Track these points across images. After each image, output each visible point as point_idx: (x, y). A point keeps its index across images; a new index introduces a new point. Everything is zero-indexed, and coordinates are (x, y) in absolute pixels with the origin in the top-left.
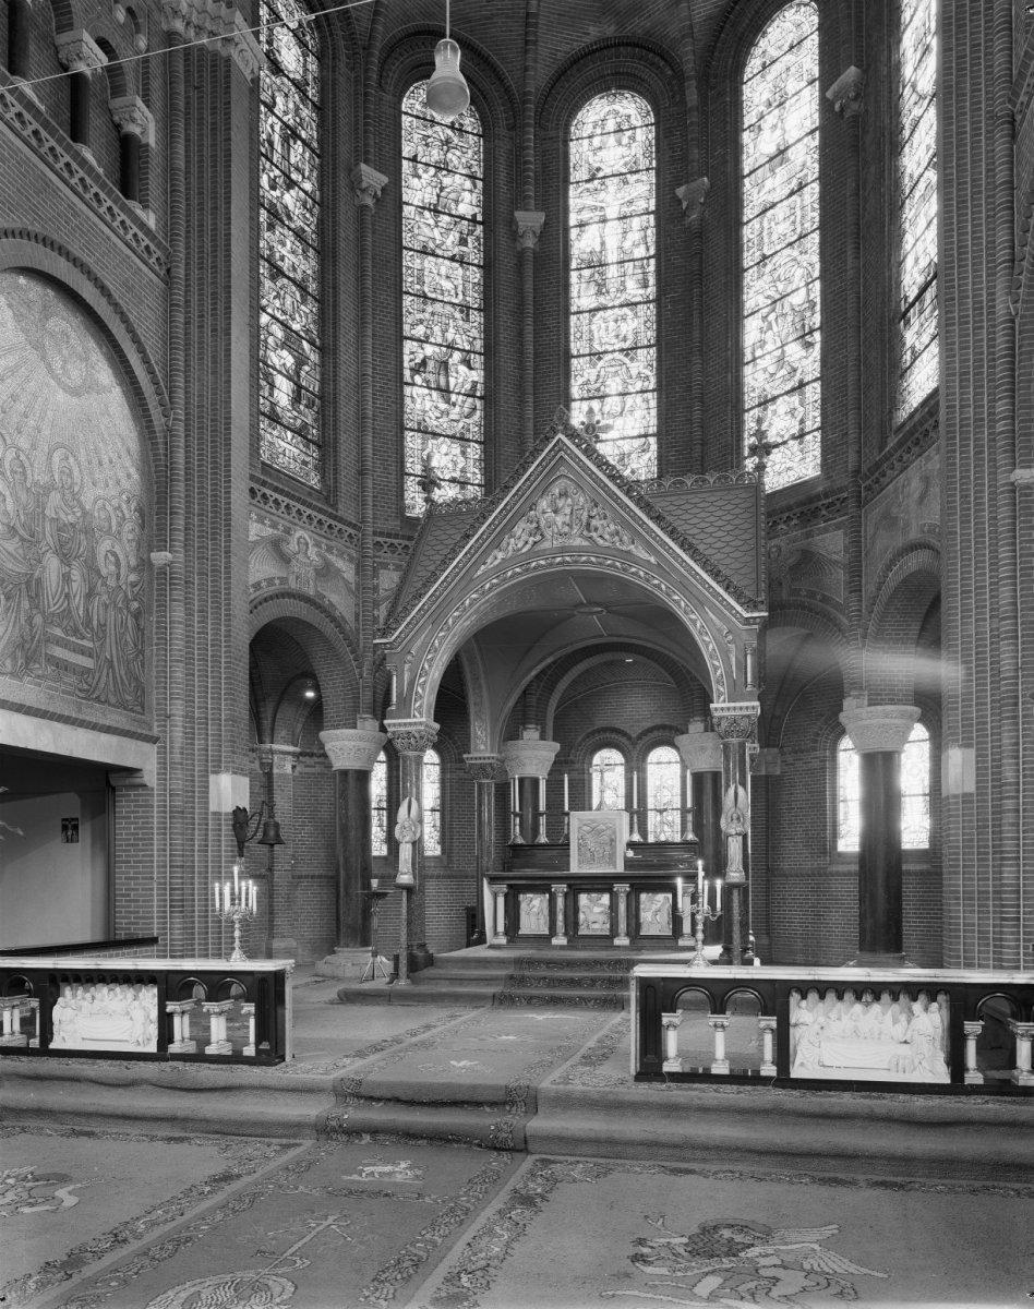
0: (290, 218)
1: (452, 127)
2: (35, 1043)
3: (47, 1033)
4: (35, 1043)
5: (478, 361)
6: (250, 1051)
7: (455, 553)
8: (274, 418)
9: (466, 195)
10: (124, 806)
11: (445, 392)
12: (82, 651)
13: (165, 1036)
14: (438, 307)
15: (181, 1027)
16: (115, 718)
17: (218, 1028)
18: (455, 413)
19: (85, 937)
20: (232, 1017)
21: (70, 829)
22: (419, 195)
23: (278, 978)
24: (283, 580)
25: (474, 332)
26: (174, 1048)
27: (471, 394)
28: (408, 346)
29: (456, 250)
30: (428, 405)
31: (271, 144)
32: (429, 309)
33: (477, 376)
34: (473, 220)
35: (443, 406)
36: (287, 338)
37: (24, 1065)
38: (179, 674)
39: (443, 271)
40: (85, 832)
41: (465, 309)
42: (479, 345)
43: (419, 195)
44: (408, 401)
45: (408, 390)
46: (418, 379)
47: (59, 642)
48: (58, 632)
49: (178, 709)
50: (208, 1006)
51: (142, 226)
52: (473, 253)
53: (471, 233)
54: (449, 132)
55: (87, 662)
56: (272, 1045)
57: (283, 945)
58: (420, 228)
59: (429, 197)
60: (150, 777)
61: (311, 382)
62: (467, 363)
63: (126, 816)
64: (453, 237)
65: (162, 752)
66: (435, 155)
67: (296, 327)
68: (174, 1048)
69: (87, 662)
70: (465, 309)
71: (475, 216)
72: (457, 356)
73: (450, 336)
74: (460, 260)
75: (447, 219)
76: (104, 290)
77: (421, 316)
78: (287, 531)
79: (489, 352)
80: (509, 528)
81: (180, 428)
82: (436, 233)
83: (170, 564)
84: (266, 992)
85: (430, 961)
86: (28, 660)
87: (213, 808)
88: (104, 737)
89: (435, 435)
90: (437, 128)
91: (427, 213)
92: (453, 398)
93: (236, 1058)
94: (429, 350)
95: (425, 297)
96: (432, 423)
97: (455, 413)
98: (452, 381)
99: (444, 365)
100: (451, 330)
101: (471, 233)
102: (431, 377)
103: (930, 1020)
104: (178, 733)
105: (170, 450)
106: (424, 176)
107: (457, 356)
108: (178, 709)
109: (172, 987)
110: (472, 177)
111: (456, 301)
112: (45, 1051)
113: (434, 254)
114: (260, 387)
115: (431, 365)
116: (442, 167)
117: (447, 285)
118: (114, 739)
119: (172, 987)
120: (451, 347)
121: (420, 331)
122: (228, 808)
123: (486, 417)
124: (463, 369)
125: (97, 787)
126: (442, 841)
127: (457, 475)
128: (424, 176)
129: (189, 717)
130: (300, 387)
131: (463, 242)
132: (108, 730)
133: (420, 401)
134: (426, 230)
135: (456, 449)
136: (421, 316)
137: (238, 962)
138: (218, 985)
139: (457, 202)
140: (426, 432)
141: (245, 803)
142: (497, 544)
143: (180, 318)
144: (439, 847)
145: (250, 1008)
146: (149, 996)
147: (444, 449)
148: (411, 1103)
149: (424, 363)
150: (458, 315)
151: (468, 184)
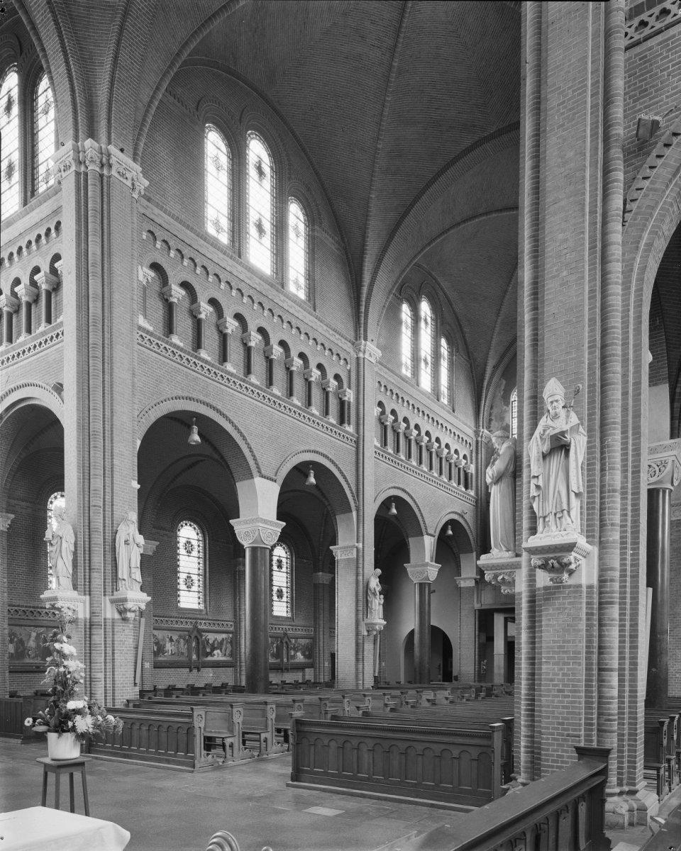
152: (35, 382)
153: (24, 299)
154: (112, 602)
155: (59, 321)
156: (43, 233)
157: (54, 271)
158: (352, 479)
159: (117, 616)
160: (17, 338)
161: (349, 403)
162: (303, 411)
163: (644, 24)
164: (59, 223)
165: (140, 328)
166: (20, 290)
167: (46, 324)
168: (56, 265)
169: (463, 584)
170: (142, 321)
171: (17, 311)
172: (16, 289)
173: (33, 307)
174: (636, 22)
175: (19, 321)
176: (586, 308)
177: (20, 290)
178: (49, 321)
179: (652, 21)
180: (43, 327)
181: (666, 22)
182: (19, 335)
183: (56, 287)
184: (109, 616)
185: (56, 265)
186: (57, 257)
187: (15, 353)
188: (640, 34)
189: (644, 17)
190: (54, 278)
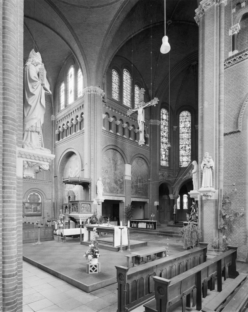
0: (164, 136)
1: (187, 116)
2: (137, 227)
3: (138, 226)
4: (137, 227)
5: (190, 145)
6: (153, 228)
7: (182, 174)
8: (162, 160)
9: (189, 124)
10: (146, 205)
11: (185, 150)
12: (141, 191)
13: (147, 227)
14: (185, 140)
15: (148, 226)
16: (144, 197)
17: (151, 226)
18: (187, 153)
19: (142, 219)
20: (152, 226)
21: (141, 207)
22: (182, 126)
23: (156, 222)
24: (163, 179)
25: (190, 142)
26: (147, 228)
27: (189, 150)
28: (180, 146)
29: (187, 132)
30: (183, 152)
31: (162, 129)
32: (183, 140)
33: (190, 147)
34: (190, 127)
35: (185, 152)
36: (164, 150)
37: (136, 229)
38: (151, 191)
39: (185, 135)
40: (142, 208)
41: (188, 139)
42: (190, 143)
43: (182, 126)
44: (180, 152)
45: (180, 151)
46: (182, 149)
47: (139, 190)
48: (139, 190)
49: (151, 195)
50: (150, 225)
51: (147, 147)
52: (190, 131)
53: (189, 129)
54: (186, 117)
55: (142, 192)
56: (155, 228)
57: (166, 220)
58: (182, 130)
59: (183, 126)
60: (148, 202)
61: (167, 154)
62: (189, 146)
63: (146, 207)
64: (187, 130)
65: (149, 200)
66: (184, 120)
67: (165, 148)
68: (147, 228)
69: (142, 192)
70: (188, 139)
71: (190, 126)
72: (187, 145)
73: (186, 143)
74: (188, 133)
75: (186, 128)
76: (144, 155)
77: (182, 141)
78: (164, 173)
79: (192, 144)
80: (186, 174)
81: (151, 166)
82: (184, 130)
83: (150, 180)
84: (155, 223)
85: (178, 222)
86: (137, 193)
87: (155, 205)
88: (144, 199)
89: (184, 156)
90: (185, 117)
91: (183, 128)
92: (187, 151)
93: (152, 229)
94: (183, 145)
95: (183, 139)
96: (184, 155)
97: (187, 153)
98: (186, 149)
99: (185, 147)
100: (186, 142)
101: (189, 129)
102: (184, 149)
103: (145, 224)
104: (151, 197)
105: (150, 168)
106: (183, 124)
107: (187, 145)
108: (151, 195)
109: (148, 223)
110: (189, 122)
111: (187, 138)
112: (138, 228)
113: (184, 133)
114: (160, 157)
115: (183, 147)
116: (186, 121)
117: (186, 136)
118: (144, 199)
119: (148, 223)
120: (186, 144)
121: (182, 143)
122: (156, 205)
123: (191, 152)
124: (188, 147)
125: (144, 203)
126: (180, 207)
127: (187, 161)
128: (183, 124)
129: (152, 196)
130: (166, 155)
131: (188, 130)
132: (144, 198)
133: (182, 152)
134: (183, 130)
135: (187, 157)
136: (182, 141)
137: (153, 221)
138: (151, 223)
139: (187, 125)
140: (182, 156)
141: (158, 205)
142: (185, 175)
143: (151, 154)
144: (180, 208)
145: (153, 225)
146: (146, 223)
147: (185, 158)
148: (165, 233)
149: (182, 147)
150: (187, 140)
151: (189, 123)
152: (73, 148)
153: (65, 129)
154: (96, 200)
155: (83, 129)
156: (77, 109)
157: (82, 117)
159: (97, 203)
160: (64, 138)
162: (133, 142)
163: (229, 62)
164: (83, 105)
165: (103, 130)
166: (78, 119)
167: (75, 132)
168: (82, 116)
169: (140, 144)
170: (103, 128)
171: (68, 129)
172: (68, 124)
173: (76, 125)
174: (228, 62)
175: (73, 129)
176: (215, 133)
177: (78, 119)
178: (80, 129)
179: (237, 59)
180: (79, 131)
181: (241, 60)
182: (73, 133)
183: (82, 120)
184: (95, 203)
185: (82, 116)
186: (82, 114)
187: (64, 141)
188: (234, 62)
189: (230, 61)
190: (67, 126)
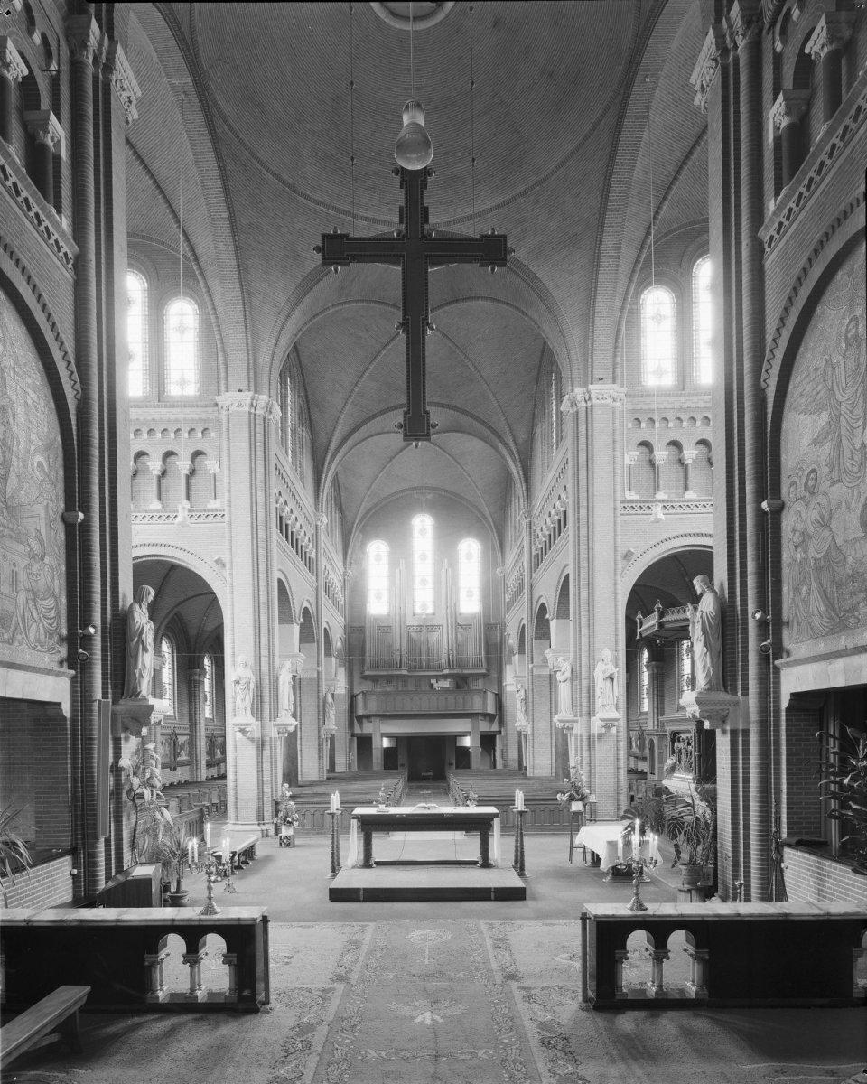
158: (70, 345)
161: (57, 158)
